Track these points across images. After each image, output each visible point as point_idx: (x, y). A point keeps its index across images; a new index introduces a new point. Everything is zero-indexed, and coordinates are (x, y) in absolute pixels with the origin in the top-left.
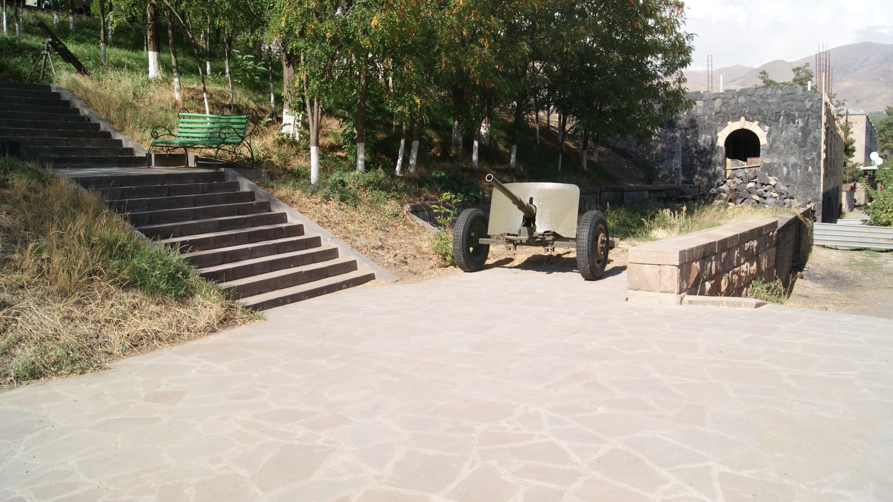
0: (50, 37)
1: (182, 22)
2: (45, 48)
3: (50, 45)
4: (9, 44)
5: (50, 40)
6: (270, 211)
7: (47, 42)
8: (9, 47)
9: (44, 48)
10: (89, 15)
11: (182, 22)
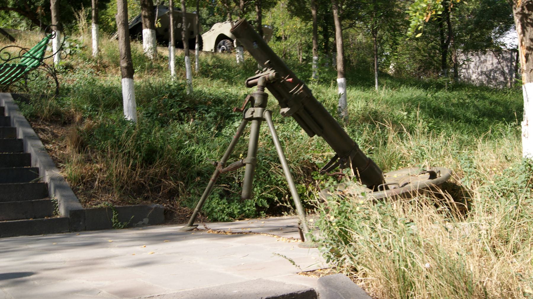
0: (270, 66)
1: (357, 170)
2: (257, 100)
3: (267, 91)
4: (171, 97)
5: (270, 73)
6: (152, 209)
7: (260, 82)
8: (171, 102)
9: (252, 99)
10: (237, 127)
11: (357, 170)
